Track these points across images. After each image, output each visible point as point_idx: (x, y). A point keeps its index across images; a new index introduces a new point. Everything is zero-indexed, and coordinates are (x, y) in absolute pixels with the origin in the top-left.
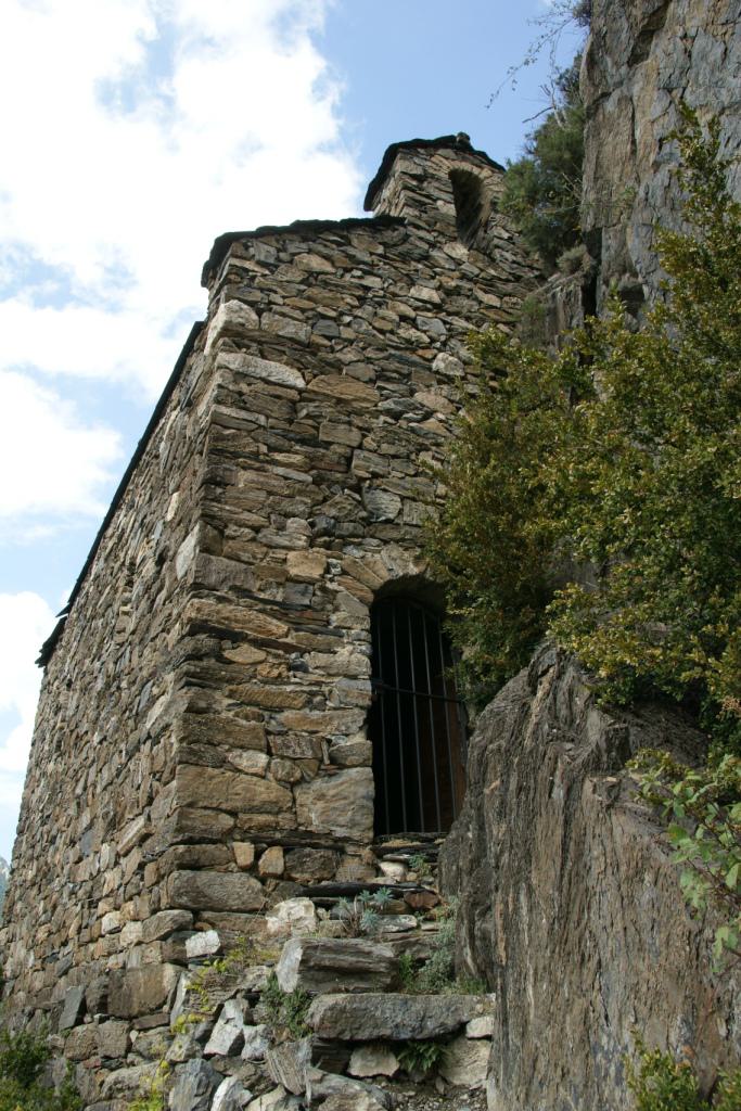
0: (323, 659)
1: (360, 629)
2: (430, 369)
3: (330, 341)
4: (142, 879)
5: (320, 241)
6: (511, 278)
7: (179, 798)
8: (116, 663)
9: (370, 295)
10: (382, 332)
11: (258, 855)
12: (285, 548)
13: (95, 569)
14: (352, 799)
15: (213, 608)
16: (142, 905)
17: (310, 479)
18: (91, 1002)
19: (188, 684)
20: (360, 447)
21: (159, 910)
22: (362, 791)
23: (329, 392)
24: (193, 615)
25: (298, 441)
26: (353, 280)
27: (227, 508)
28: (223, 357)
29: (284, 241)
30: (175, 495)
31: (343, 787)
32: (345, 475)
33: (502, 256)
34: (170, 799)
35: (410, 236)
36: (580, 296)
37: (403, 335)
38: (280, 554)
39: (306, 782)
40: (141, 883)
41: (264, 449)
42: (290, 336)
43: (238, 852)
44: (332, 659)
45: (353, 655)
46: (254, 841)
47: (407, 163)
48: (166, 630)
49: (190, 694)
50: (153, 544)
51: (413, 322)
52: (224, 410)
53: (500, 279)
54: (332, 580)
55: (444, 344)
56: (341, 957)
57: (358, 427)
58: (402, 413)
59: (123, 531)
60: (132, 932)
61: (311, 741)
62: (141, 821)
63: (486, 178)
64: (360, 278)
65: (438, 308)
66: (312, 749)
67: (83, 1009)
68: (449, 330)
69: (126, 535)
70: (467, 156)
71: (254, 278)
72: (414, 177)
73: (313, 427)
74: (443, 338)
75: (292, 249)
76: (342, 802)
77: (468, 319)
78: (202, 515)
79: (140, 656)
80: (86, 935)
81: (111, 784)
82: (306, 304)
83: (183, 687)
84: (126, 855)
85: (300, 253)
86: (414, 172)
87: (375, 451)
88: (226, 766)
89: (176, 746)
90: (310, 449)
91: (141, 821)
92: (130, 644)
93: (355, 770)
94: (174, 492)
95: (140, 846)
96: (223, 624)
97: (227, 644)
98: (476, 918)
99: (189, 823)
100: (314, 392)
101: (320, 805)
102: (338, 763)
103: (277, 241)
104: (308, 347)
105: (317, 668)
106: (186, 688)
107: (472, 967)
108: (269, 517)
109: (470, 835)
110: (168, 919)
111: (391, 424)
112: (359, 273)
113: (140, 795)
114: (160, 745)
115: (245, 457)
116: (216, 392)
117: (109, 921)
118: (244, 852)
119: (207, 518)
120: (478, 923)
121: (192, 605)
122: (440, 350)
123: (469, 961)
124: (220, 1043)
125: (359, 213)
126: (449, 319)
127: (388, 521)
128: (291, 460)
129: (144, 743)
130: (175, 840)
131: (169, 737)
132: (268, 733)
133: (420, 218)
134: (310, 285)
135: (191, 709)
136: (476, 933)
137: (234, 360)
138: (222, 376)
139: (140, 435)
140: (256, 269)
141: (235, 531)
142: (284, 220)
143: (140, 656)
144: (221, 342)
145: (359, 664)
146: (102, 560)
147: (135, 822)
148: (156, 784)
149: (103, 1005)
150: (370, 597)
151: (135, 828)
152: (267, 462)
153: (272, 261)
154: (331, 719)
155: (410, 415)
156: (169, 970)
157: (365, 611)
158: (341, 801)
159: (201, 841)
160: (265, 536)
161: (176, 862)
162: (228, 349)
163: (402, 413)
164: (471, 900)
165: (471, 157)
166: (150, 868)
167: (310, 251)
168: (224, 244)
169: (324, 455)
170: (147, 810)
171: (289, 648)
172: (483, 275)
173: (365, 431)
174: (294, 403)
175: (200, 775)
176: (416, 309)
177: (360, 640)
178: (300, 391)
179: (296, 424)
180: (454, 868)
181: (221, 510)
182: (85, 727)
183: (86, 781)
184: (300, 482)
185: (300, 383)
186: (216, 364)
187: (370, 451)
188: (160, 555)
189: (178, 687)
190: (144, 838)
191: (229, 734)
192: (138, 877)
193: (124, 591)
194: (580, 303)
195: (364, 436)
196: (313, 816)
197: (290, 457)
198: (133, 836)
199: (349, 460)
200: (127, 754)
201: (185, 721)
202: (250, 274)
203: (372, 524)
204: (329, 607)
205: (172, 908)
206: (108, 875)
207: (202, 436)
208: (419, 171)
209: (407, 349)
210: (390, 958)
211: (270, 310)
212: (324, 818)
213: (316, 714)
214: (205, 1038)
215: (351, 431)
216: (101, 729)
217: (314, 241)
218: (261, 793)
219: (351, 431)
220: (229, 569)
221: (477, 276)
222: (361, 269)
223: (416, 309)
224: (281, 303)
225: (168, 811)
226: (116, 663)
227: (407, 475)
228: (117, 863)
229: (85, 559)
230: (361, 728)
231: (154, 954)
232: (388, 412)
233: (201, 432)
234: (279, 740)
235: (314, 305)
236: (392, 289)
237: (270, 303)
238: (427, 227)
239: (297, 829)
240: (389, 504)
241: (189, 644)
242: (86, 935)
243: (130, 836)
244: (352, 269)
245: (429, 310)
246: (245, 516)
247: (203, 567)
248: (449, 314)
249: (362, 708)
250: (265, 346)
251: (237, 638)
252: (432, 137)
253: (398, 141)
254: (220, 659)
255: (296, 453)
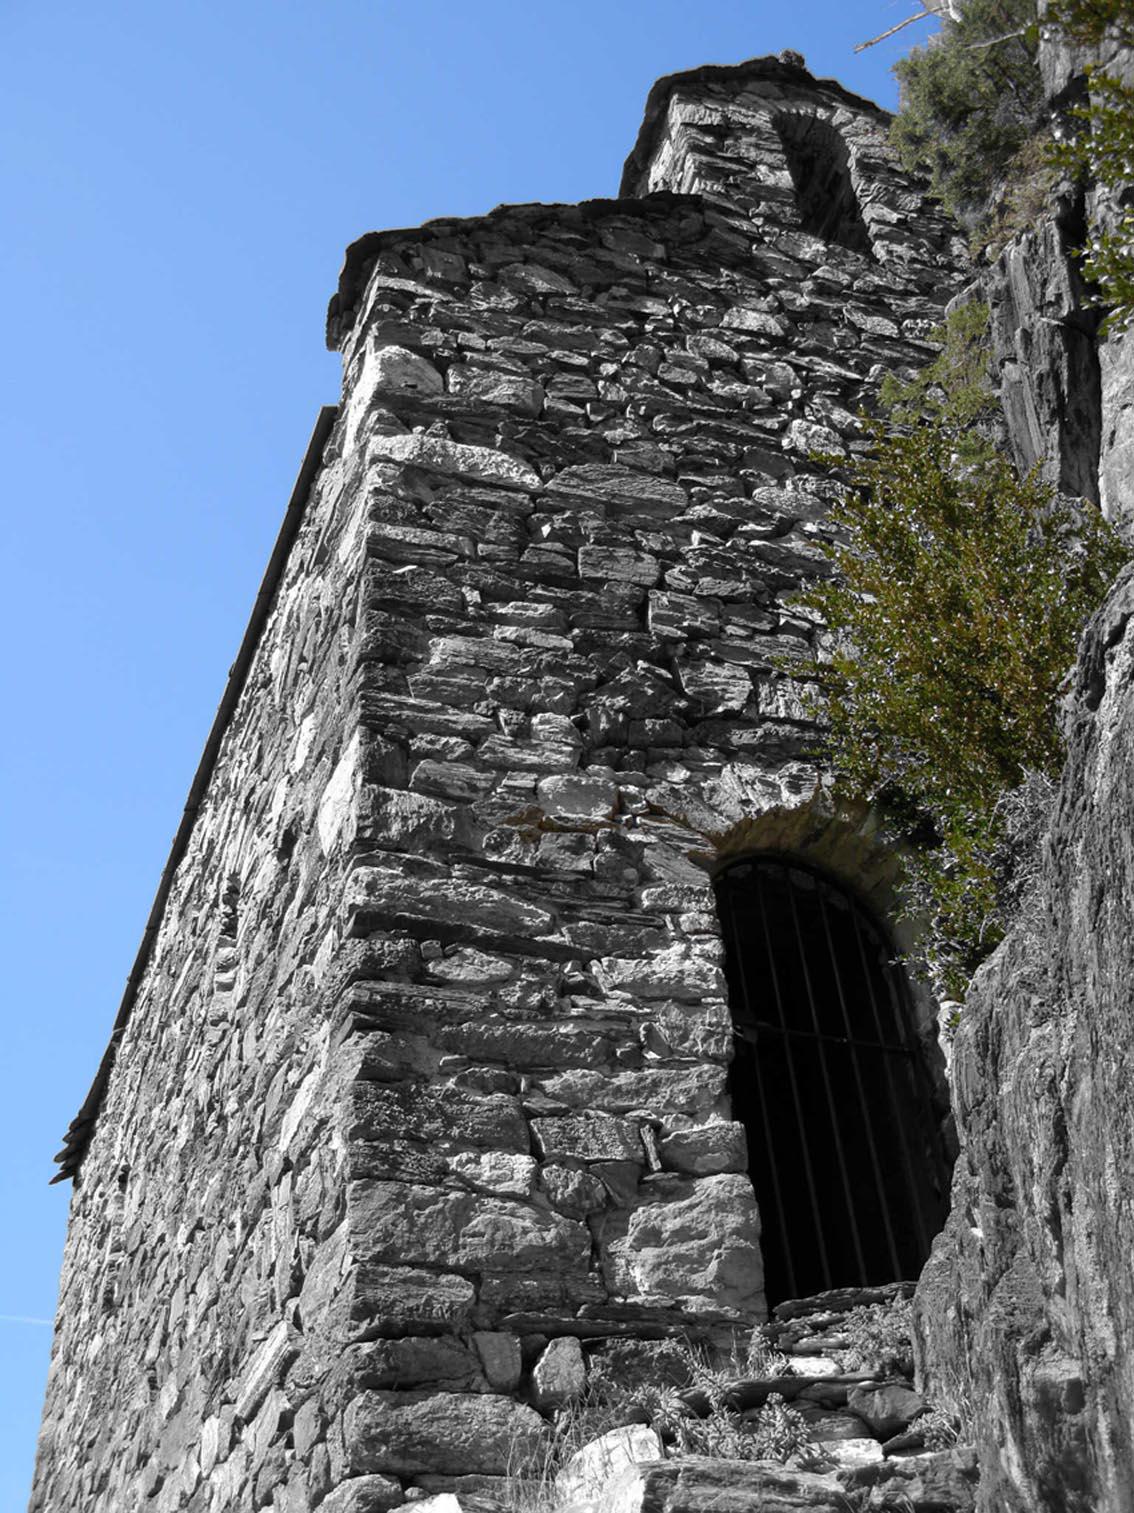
0: (628, 969)
1: (697, 914)
2: (779, 447)
3: (583, 407)
4: (290, 1445)
5: (544, 241)
6: (911, 287)
7: (356, 1246)
8: (211, 1077)
9: (649, 327)
10: (680, 388)
11: (530, 1359)
12: (531, 768)
13: (161, 943)
14: (714, 1236)
15: (399, 882)
17: (568, 644)
19: (361, 1027)
20: (661, 585)
21: (330, 1487)
22: (733, 1220)
23: (589, 494)
24: (360, 900)
25: (537, 581)
26: (611, 303)
27: (412, 701)
28: (378, 444)
29: (477, 246)
30: (309, 722)
31: (695, 1213)
32: (637, 635)
33: (890, 252)
34: (336, 1261)
35: (712, 226)
36: (1057, 238)
37: (720, 392)
38: (526, 781)
39: (616, 1208)
40: (288, 1454)
41: (473, 596)
42: (505, 401)
43: (487, 1351)
44: (647, 970)
45: (687, 958)
46: (518, 1329)
47: (690, 107)
48: (308, 958)
49: (366, 1044)
50: (272, 828)
51: (736, 371)
52: (390, 531)
53: (891, 291)
54: (632, 826)
55: (800, 404)
56: (732, 1492)
57: (651, 552)
58: (734, 525)
59: (211, 842)
61: (619, 1127)
63: (843, 124)
64: (624, 299)
65: (780, 344)
66: (624, 1142)
68: (805, 380)
69: (217, 850)
70: (803, 90)
71: (425, 308)
72: (706, 129)
73: (564, 555)
74: (796, 394)
75: (493, 257)
76: (695, 1243)
77: (841, 361)
78: (363, 720)
79: (258, 1038)
81: (214, 1302)
82: (533, 347)
83: (349, 1036)
84: (249, 1420)
85: (508, 263)
86: (707, 121)
87: (690, 592)
88: (450, 1181)
89: (342, 1152)
90: (560, 593)
92: (238, 1026)
93: (714, 1179)
94: (304, 716)
95: (281, 1385)
96: (421, 912)
97: (430, 945)
98: (1021, 1359)
99: (381, 1294)
100: (560, 494)
101: (649, 1253)
102: (680, 1170)
103: (465, 245)
104: (541, 419)
105: (615, 987)
106: (356, 1035)
107: (1024, 1492)
108: (495, 716)
109: (978, 1232)
110: (348, 1497)
111: (715, 545)
112: (624, 291)
113: (275, 1285)
114: (310, 1168)
115: (437, 611)
116: (371, 502)
118: (500, 1351)
119: (373, 724)
120: (1027, 1370)
121: (356, 880)
122: (793, 415)
123: (1016, 1475)
125: (612, 192)
126: (804, 361)
127: (730, 715)
128: (530, 613)
129: (278, 1182)
130: (353, 1335)
131: (330, 1139)
132: (529, 1114)
133: (727, 196)
134: (533, 316)
135: (370, 1072)
136: (1024, 1395)
137: (404, 446)
138: (381, 474)
139: (234, 659)
140: (428, 292)
141: (431, 742)
142: (473, 205)
143: (258, 1038)
144: (374, 416)
145: (701, 975)
146: (174, 917)
147: (268, 1342)
148: (306, 1243)
152: (481, 619)
153: (456, 277)
154: (656, 1084)
155: (751, 526)
157: (701, 879)
158: (692, 1237)
159: (405, 1332)
160: (491, 750)
161: (358, 1375)
162: (387, 428)
163: (734, 525)
164: (1004, 1326)
165: (811, 93)
167: (526, 260)
168: (366, 254)
169: (591, 602)
170: (292, 1304)
171: (559, 953)
172: (857, 284)
173: (668, 558)
175: (400, 1198)
176: (739, 347)
177: (697, 932)
178: (534, 496)
179: (524, 557)
180: (951, 1313)
181: (401, 706)
182: (160, 1227)
183: (167, 1322)
184: (548, 650)
185: (532, 480)
186: (367, 458)
187: (682, 592)
188: (287, 833)
189: (340, 1036)
191: (450, 1121)
192: (282, 1442)
193: (221, 944)
194: (1057, 250)
195: (664, 568)
196: (637, 1273)
197: (526, 608)
198: (266, 1370)
199: (641, 609)
200: (244, 1227)
201: (358, 1096)
202: (418, 300)
203: (702, 730)
204: (631, 873)
205: (355, 1474)
206: (217, 1478)
207: (351, 589)
208: (716, 119)
209: (729, 416)
210: (836, 1494)
211: (463, 360)
212: (660, 1275)
213: (626, 1078)
215: (639, 559)
216: (191, 1211)
217: (533, 244)
218: (525, 1231)
219: (639, 559)
220: (423, 811)
221: (849, 286)
222: (625, 285)
223: (739, 347)
224: (483, 347)
225: (335, 1283)
226: (211, 1077)
227: (756, 631)
228: (234, 1442)
230: (718, 1100)
232: (704, 524)
233: (349, 583)
234: (553, 1126)
235: (545, 348)
236: (689, 314)
237: (461, 348)
238: (743, 212)
239: (605, 1303)
240: (730, 685)
241: (357, 951)
243: (259, 1374)
244: (607, 288)
245: (763, 349)
246: (452, 715)
247: (375, 815)
248: (802, 353)
249: (714, 1060)
250: (458, 422)
251: (452, 935)
252: (734, 60)
253: (670, 72)
254: (420, 977)
255: (539, 599)
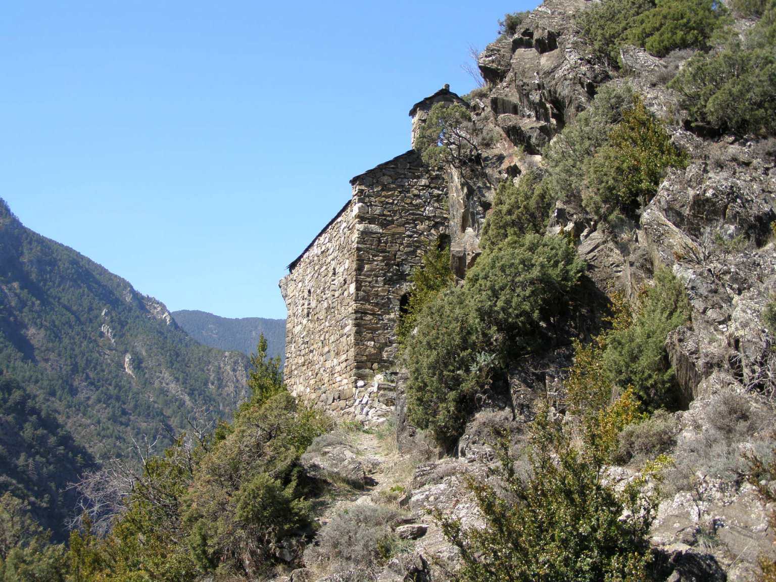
16: (347, 375)
18: (336, 397)
20: (399, 250)
60: (345, 381)
62: (345, 355)
67: (334, 399)
80: (331, 382)
91: (345, 355)
117: (339, 379)
124: (364, 401)
149: (339, 398)
150: (400, 298)
151: (344, 357)
156: (354, 389)
166: (348, 367)
174: (379, 238)
190: (346, 360)
206: (337, 367)
214: (361, 401)
229: (341, 208)
231: (351, 386)
242: (331, 382)
